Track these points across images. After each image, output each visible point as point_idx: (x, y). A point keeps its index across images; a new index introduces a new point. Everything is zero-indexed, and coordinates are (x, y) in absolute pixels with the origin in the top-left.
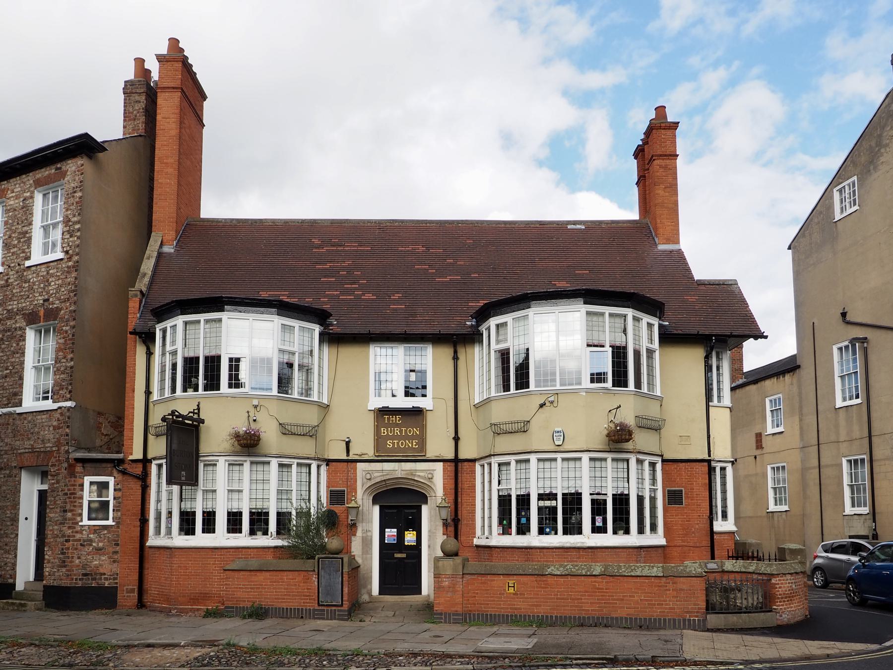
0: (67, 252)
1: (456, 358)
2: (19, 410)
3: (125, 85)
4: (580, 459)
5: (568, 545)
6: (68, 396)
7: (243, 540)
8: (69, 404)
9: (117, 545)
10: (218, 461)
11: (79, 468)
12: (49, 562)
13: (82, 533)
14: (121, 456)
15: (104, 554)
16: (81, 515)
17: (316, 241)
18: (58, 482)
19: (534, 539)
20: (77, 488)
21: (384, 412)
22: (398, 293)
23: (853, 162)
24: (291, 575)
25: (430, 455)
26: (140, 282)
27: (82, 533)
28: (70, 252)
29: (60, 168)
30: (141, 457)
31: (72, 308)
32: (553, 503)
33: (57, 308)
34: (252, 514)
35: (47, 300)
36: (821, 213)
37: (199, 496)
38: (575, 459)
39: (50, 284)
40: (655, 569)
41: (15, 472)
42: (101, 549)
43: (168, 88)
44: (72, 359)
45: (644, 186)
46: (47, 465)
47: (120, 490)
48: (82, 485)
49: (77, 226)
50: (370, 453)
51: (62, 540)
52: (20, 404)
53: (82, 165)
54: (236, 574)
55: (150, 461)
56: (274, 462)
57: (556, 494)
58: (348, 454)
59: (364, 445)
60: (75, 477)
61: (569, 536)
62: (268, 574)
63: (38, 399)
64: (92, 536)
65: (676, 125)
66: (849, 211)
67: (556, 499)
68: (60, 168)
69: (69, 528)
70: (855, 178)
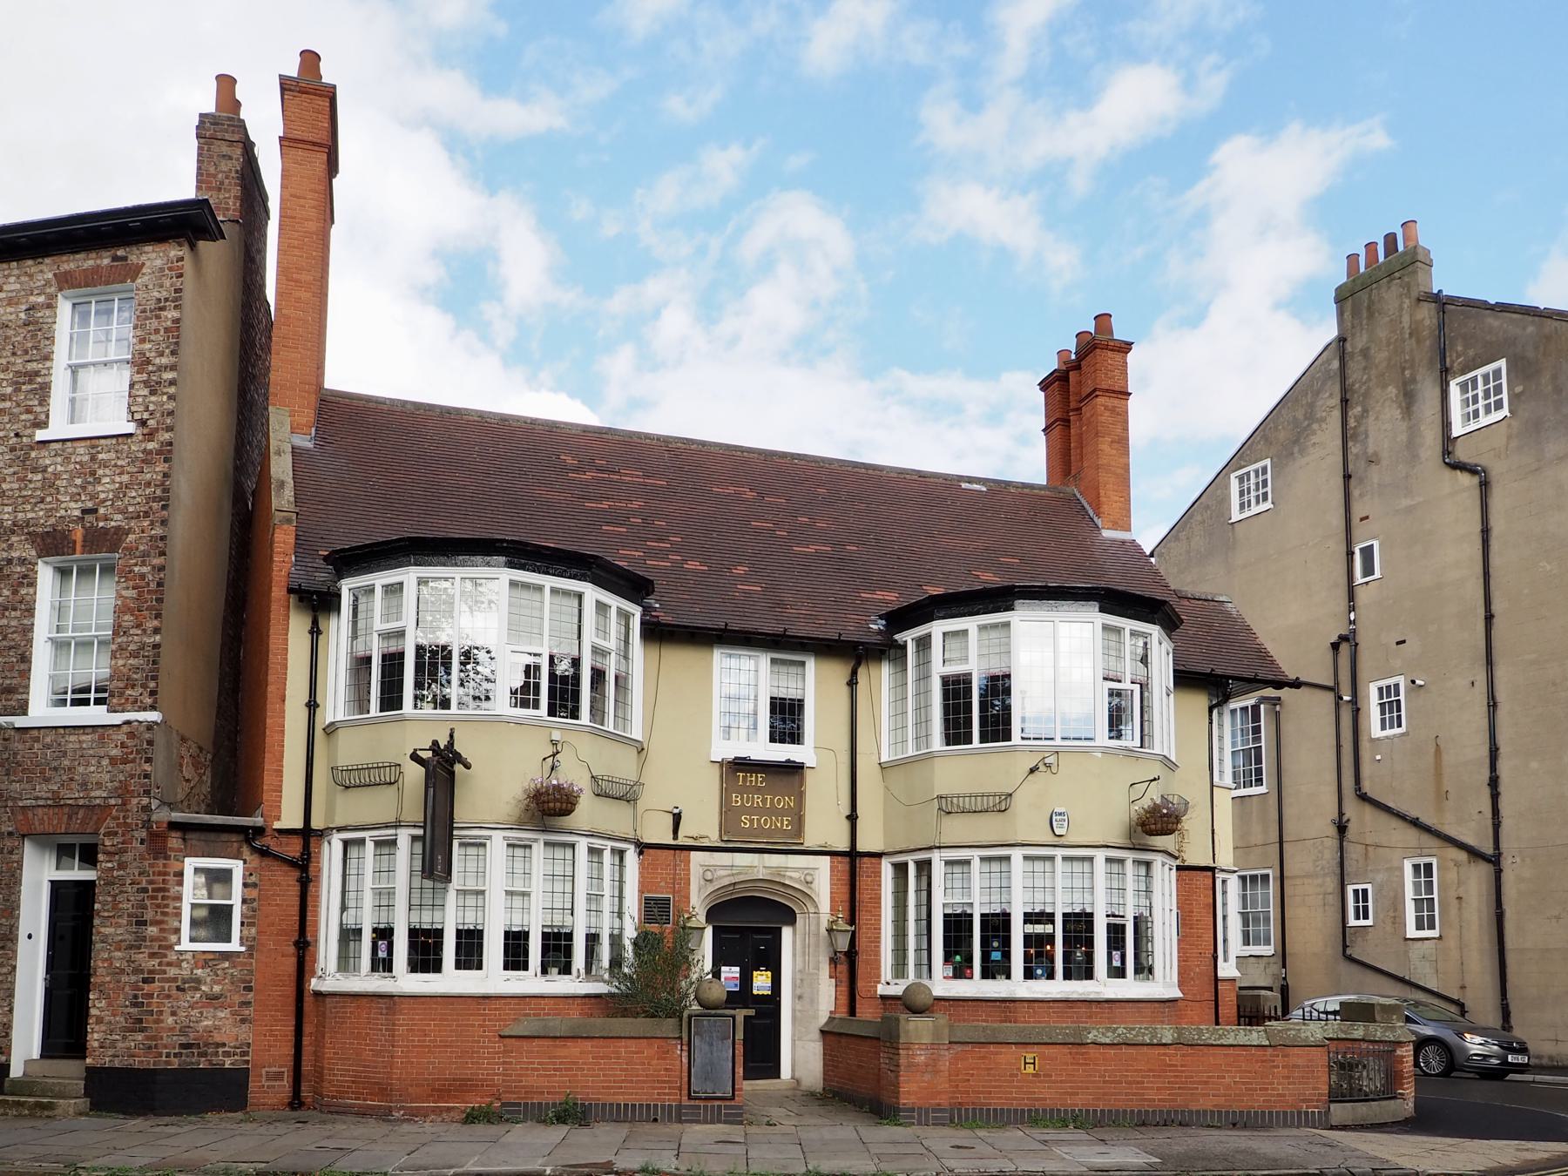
0: (143, 423)
1: (852, 683)
2: (20, 722)
3: (201, 122)
4: (1008, 858)
5: (1075, 996)
6: (149, 701)
7: (530, 982)
8: (154, 716)
9: (249, 989)
10: (490, 838)
11: (174, 841)
12: (100, 1020)
13: (180, 966)
14: (258, 821)
15: (223, 1007)
16: (177, 931)
17: (569, 460)
18: (122, 866)
19: (1017, 986)
20: (171, 878)
21: (740, 765)
22: (740, 564)
23: (1265, 438)
24: (633, 1045)
25: (810, 842)
26: (278, 496)
27: (180, 966)
28: (152, 423)
29: (125, 259)
30: (298, 824)
31: (158, 531)
32: (1049, 929)
33: (118, 528)
34: (545, 936)
35: (94, 511)
36: (1208, 507)
37: (451, 896)
38: (1083, 859)
39: (98, 481)
40: (1255, 1034)
41: (8, 843)
42: (216, 998)
43: (303, 142)
44: (156, 631)
45: (1066, 439)
46: (96, 833)
47: (255, 885)
48: (181, 874)
49: (168, 375)
50: (713, 838)
51: (133, 978)
52: (23, 709)
53: (181, 259)
54: (525, 1044)
55: (322, 834)
56: (583, 844)
57: (1053, 915)
58: (675, 836)
59: (703, 823)
60: (167, 858)
61: (1073, 982)
62: (588, 1043)
63: (63, 703)
64: (199, 972)
65: (1126, 347)
66: (1255, 509)
67: (1053, 922)
68: (125, 259)
69: (152, 955)
70: (1268, 462)
